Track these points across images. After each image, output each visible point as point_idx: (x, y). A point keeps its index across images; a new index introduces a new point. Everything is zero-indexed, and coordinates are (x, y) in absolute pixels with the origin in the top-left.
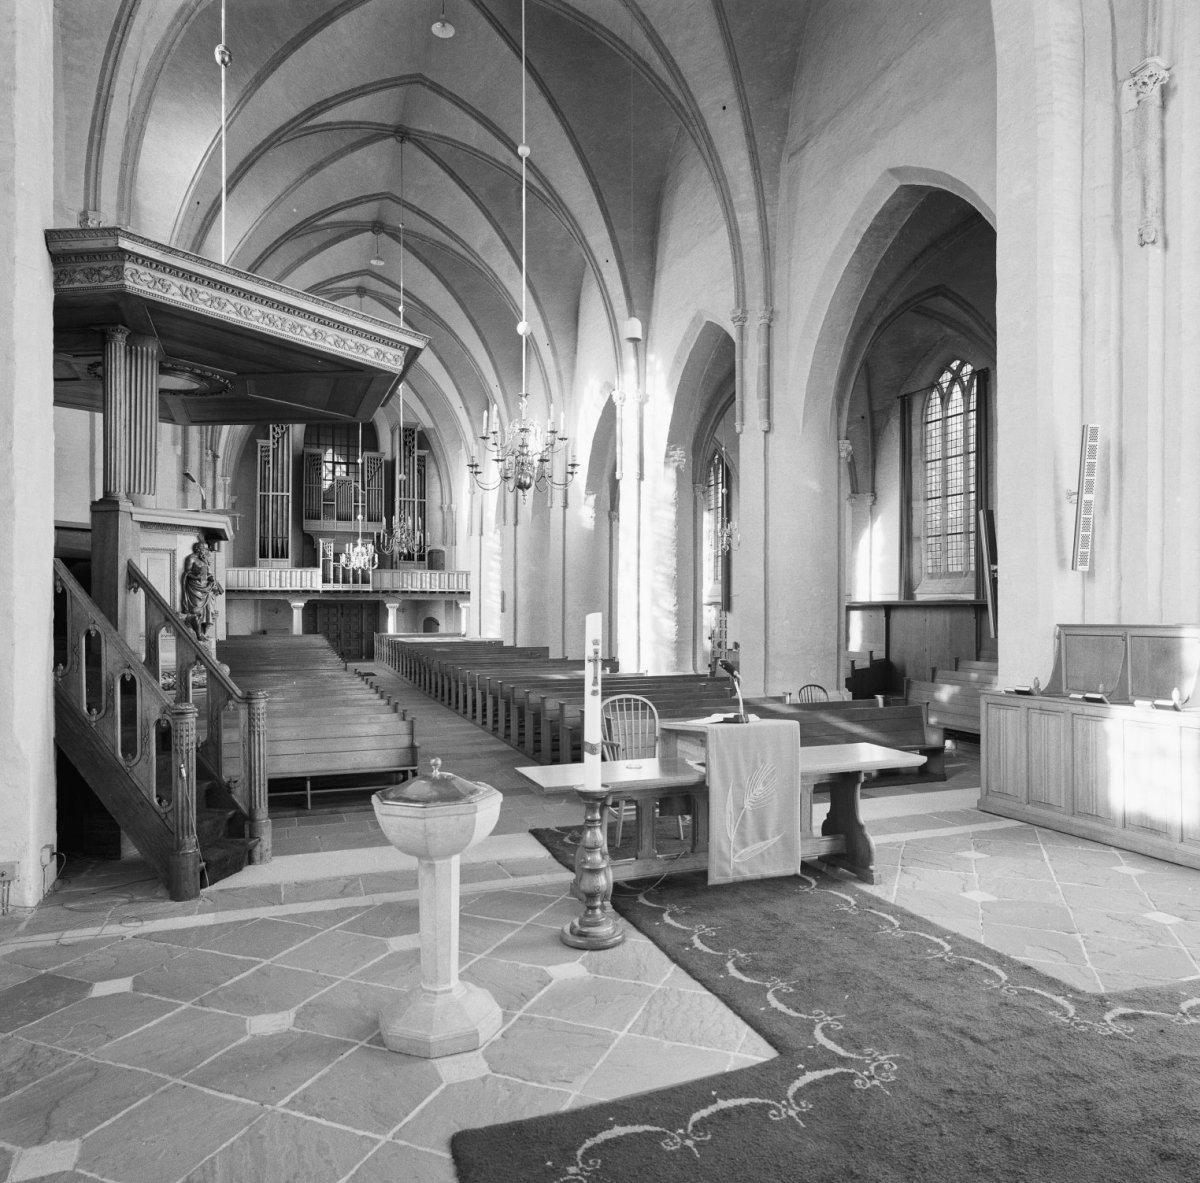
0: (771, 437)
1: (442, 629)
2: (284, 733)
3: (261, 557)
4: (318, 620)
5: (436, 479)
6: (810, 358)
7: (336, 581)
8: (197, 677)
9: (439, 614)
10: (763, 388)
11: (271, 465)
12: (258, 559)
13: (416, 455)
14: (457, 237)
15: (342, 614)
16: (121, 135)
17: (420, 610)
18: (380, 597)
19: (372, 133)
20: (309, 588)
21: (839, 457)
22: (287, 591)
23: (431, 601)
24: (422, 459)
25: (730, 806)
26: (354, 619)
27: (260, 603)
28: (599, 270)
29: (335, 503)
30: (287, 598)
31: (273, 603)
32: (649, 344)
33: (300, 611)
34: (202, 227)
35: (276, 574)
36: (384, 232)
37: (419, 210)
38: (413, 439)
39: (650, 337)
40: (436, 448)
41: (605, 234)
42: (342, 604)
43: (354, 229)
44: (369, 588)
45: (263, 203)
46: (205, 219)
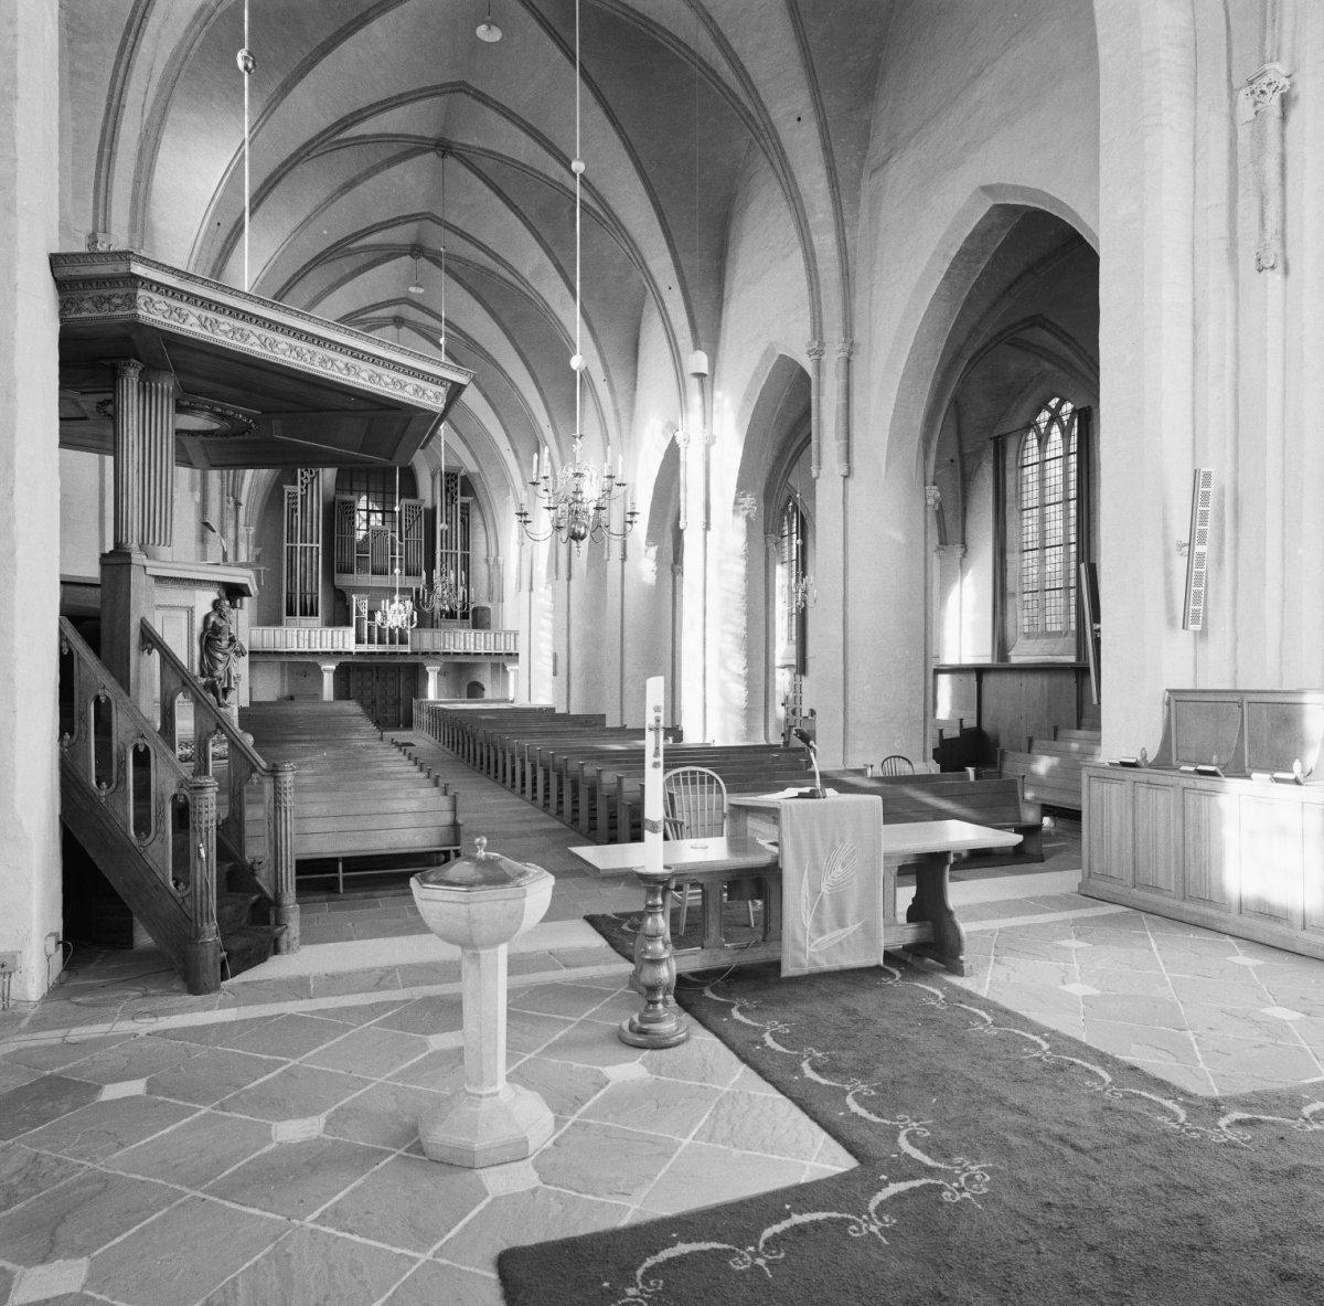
0: (851, 482)
1: (488, 694)
2: (314, 810)
3: (287, 615)
4: (351, 685)
5: (481, 529)
6: (893, 395)
7: (371, 641)
8: (217, 747)
9: (485, 677)
10: (842, 429)
11: (299, 514)
12: (285, 618)
13: (459, 502)
14: (505, 261)
15: (378, 678)
16: (134, 149)
17: (463, 673)
18: (419, 659)
19: (411, 147)
20: (340, 649)
21: (926, 505)
22: (317, 653)
23: (476, 664)
24: (465, 507)
25: (805, 890)
26: (391, 683)
27: (287, 665)
28: (661, 299)
29: (370, 555)
30: (317, 660)
31: (301, 666)
32: (716, 379)
33: (331, 675)
34: (222, 251)
35: (304, 634)
36: (424, 256)
37: (462, 232)
38: (456, 485)
39: (717, 372)
40: (481, 495)
41: (668, 259)
42: (378, 667)
43: (390, 253)
44: (407, 649)
45: (290, 224)
46: (226, 242)
